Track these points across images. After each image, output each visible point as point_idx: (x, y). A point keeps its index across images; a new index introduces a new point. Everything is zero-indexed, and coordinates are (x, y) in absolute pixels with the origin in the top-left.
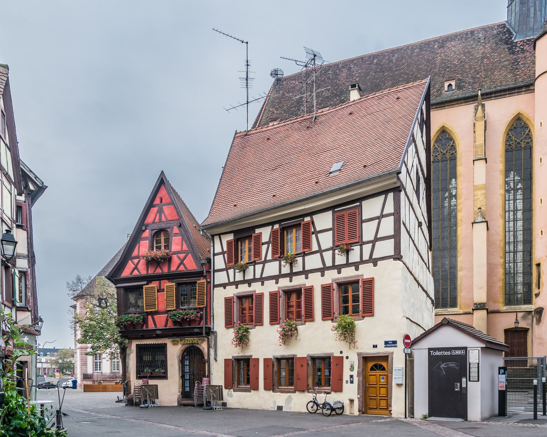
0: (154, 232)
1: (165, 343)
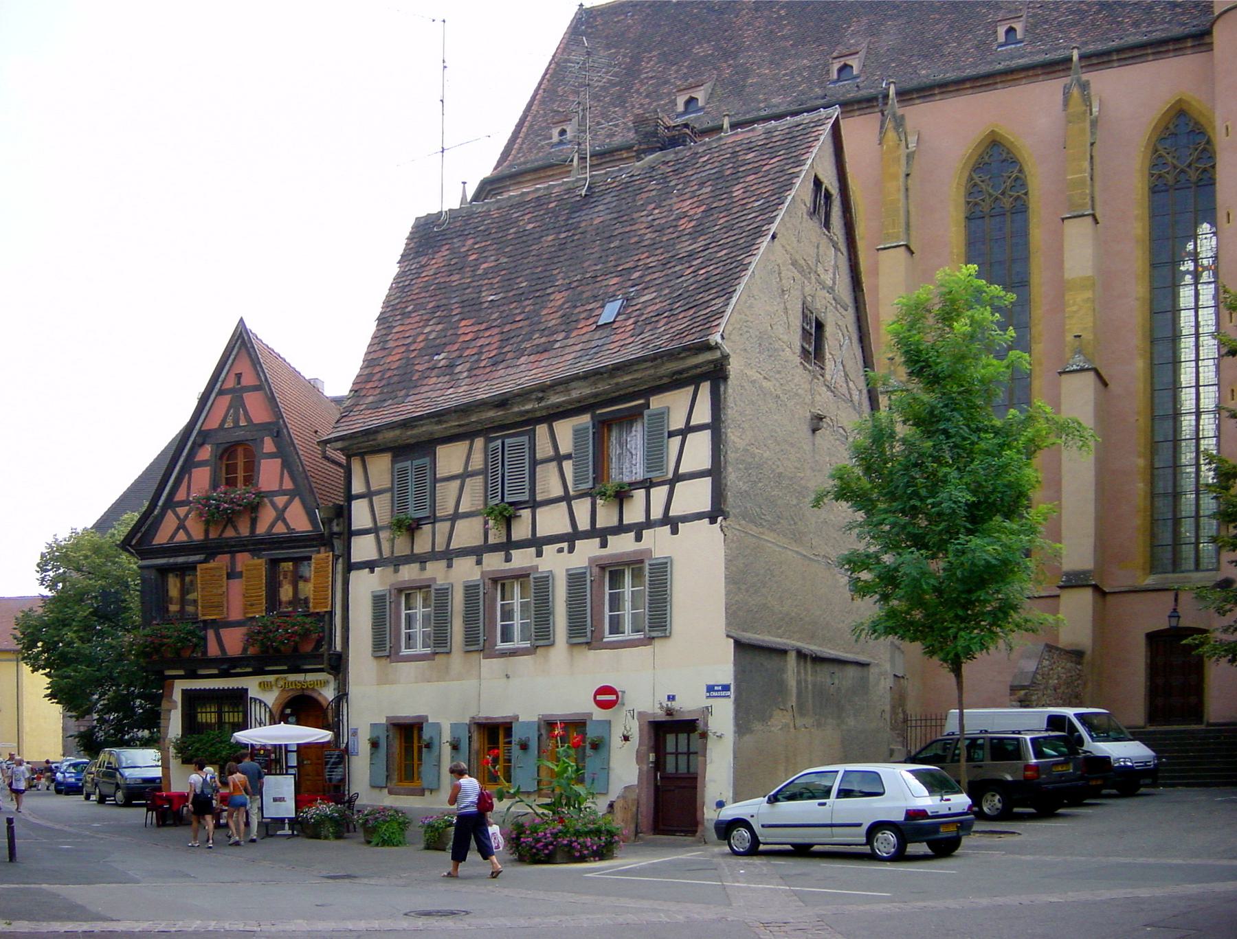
0: (223, 447)
1: (242, 689)
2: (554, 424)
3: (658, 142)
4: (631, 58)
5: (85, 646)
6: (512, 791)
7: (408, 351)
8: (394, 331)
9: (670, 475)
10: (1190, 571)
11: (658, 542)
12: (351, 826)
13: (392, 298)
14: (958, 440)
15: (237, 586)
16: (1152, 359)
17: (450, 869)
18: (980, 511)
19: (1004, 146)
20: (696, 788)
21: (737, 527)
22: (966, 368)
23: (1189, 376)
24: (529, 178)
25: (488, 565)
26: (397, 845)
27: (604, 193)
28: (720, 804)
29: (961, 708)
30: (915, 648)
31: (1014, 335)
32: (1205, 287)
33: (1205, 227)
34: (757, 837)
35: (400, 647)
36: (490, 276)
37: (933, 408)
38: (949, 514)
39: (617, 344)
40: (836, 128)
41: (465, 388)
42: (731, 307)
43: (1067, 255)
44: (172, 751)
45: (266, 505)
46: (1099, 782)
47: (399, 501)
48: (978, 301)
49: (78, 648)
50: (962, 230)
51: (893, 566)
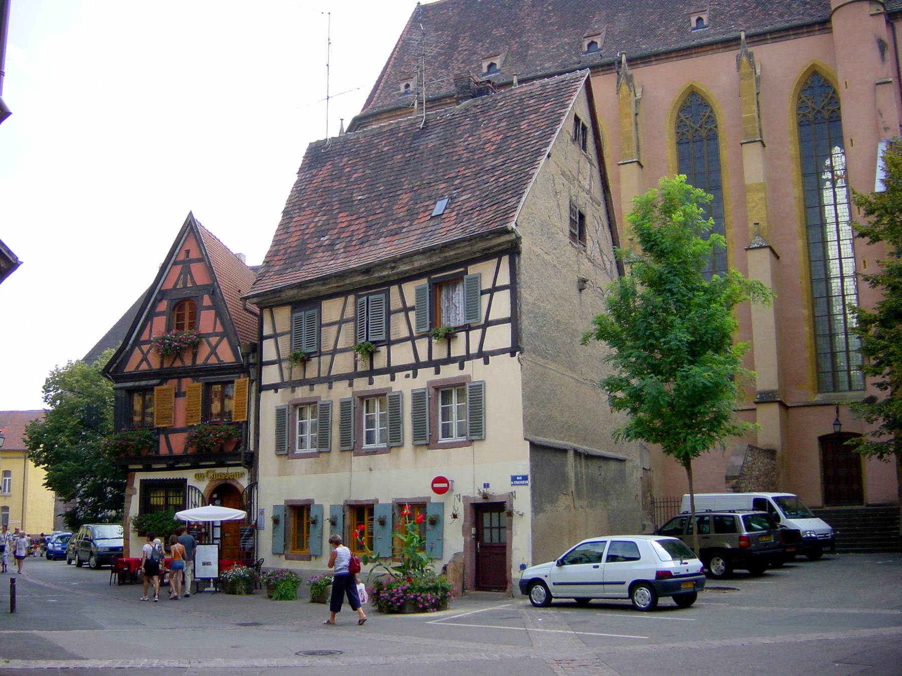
1: (183, 479)
2: (403, 285)
3: (470, 92)
5: (74, 447)
6: (374, 557)
7: (303, 234)
8: (294, 220)
9: (483, 322)
10: (846, 391)
11: (475, 370)
12: (258, 585)
14: (679, 296)
15: (182, 402)
16: (808, 239)
17: (329, 618)
18: (697, 347)
20: (505, 554)
21: (530, 359)
22: (682, 246)
24: (385, 116)
25: (357, 387)
26: (291, 599)
27: (435, 126)
28: (523, 567)
29: (692, 493)
30: (658, 448)
31: (713, 223)
32: (840, 189)
33: (837, 149)
37: (661, 274)
38: (676, 350)
40: (588, 84)
44: (132, 526)
45: (203, 343)
46: (793, 550)
47: (296, 341)
48: (688, 199)
49: (68, 448)
51: (639, 387)
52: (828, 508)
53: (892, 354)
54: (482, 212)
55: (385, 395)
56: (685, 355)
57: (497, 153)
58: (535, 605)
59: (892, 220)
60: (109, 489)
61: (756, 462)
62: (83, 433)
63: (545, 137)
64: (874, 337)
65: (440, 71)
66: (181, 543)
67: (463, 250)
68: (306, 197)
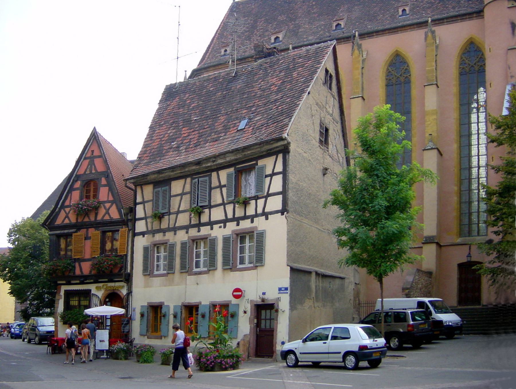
1: (89, 290)
2: (219, 172)
3: (263, 54)
4: (254, 21)
5: (26, 270)
6: (198, 337)
7: (161, 141)
8: (156, 132)
9: (266, 194)
10: (475, 236)
11: (260, 223)
12: (132, 354)
13: (155, 118)
14: (382, 178)
15: (88, 243)
16: (460, 144)
17: (171, 374)
18: (390, 209)
19: (401, 56)
20: (273, 335)
21: (292, 217)
22: (385, 148)
23: (475, 151)
24: (211, 69)
25: (191, 234)
26: (150, 363)
27: (241, 75)
28: (283, 343)
29: (382, 298)
30: (364, 271)
31: (405, 134)
32: (481, 114)
33: (482, 89)
34: (298, 359)
35: (154, 271)
36: (195, 109)
37: (372, 165)
38: (378, 211)
39: (245, 138)
40: (334, 49)
41: (183, 157)
42: (291, 122)
43: (426, 100)
44: (59, 318)
45: (101, 207)
46: (438, 333)
47: (156, 206)
48: (390, 120)
49: (22, 271)
50: (384, 90)
51: (355, 234)
52: (460, 307)
53: (505, 213)
54: (268, 127)
55: (207, 238)
56: (384, 215)
57: (279, 91)
58: (289, 366)
59: (511, 132)
60: (46, 296)
61: (420, 279)
62: (32, 262)
63: (307, 82)
64: (494, 203)
65: (246, 42)
66: (88, 329)
67: (256, 151)
68: (163, 118)
